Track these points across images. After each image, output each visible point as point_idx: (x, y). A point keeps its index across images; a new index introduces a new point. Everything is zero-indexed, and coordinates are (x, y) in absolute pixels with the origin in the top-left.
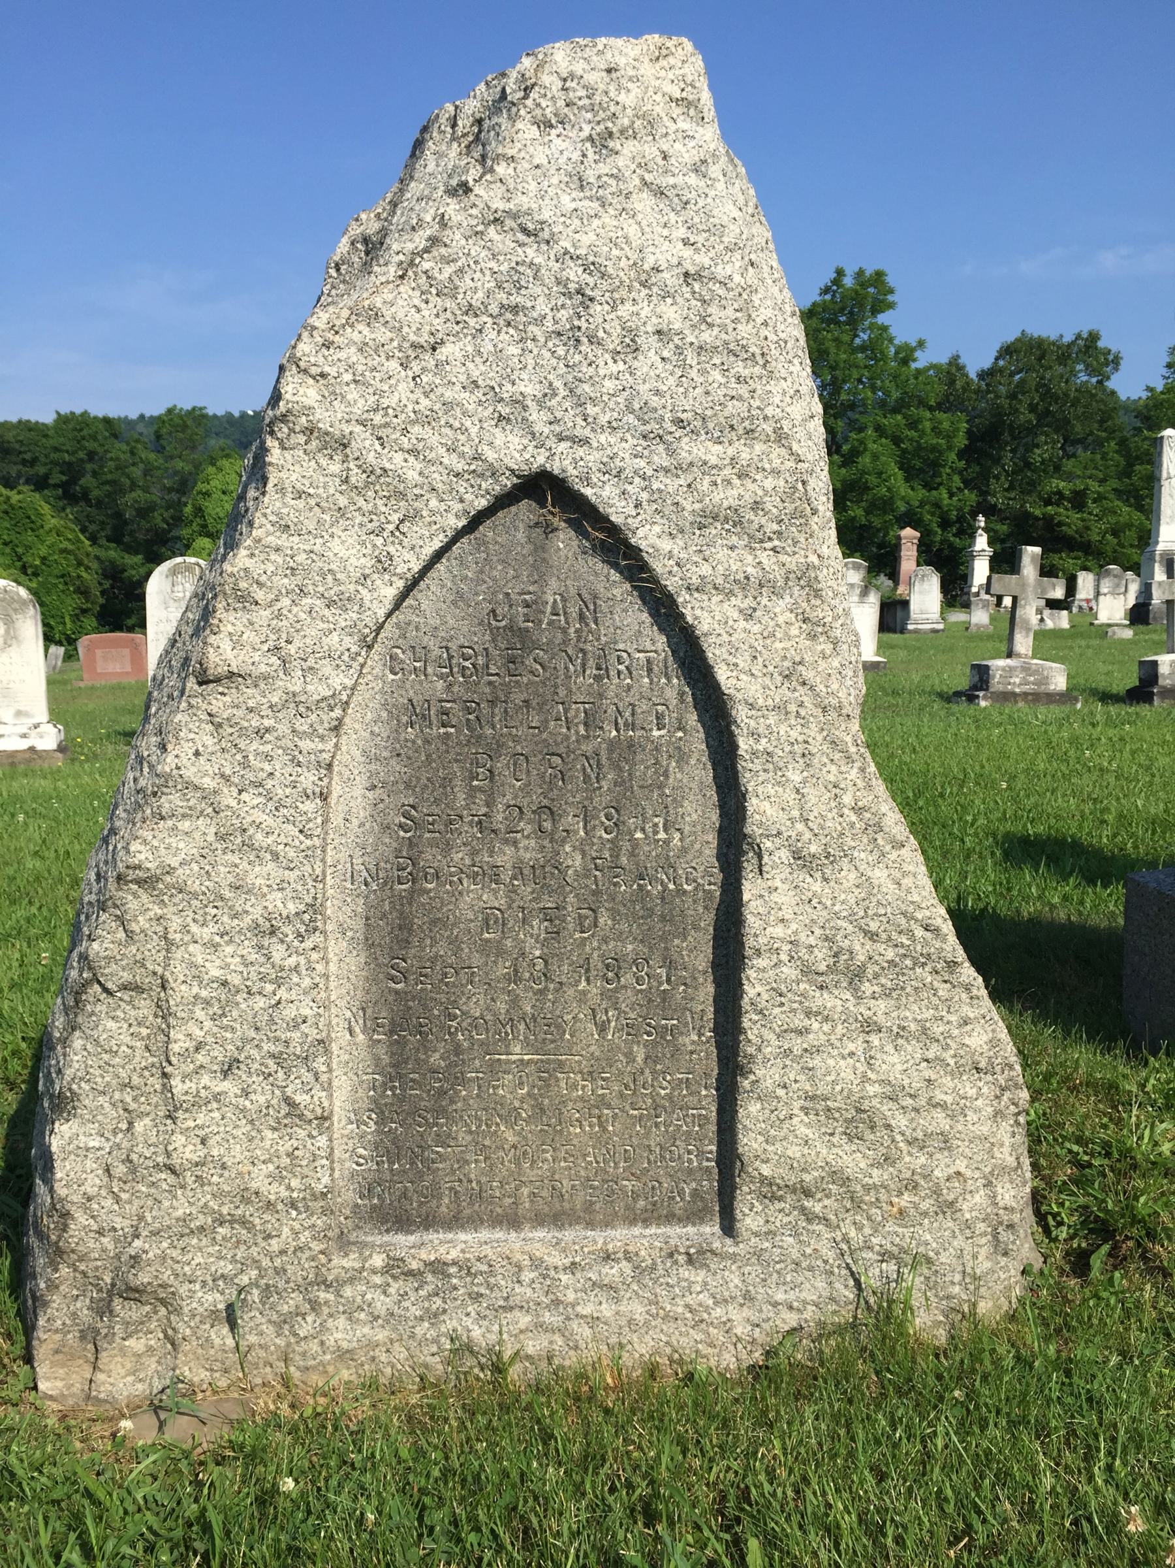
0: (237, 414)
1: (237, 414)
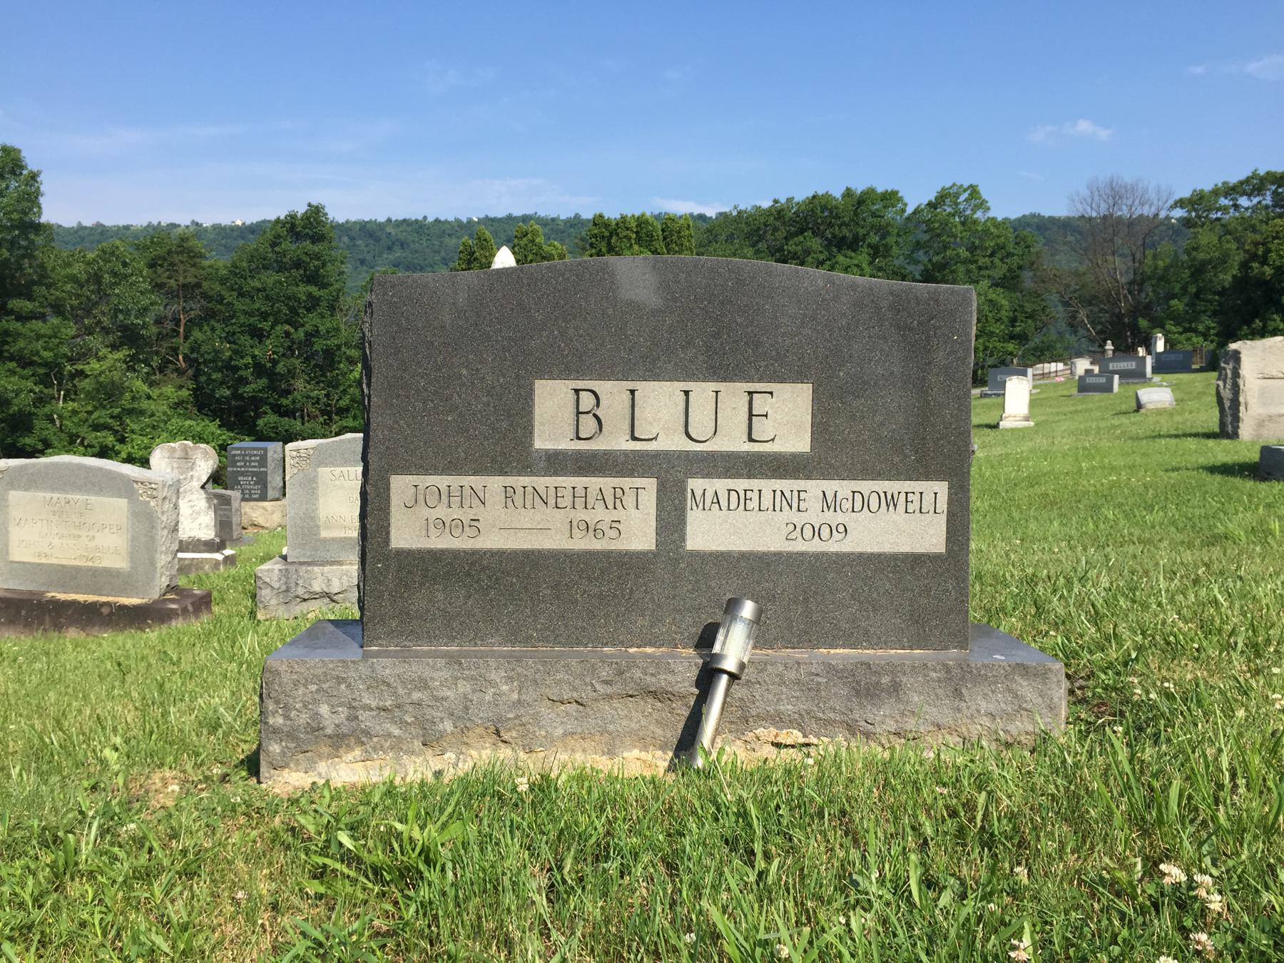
0: (465, 221)
1: (465, 221)
